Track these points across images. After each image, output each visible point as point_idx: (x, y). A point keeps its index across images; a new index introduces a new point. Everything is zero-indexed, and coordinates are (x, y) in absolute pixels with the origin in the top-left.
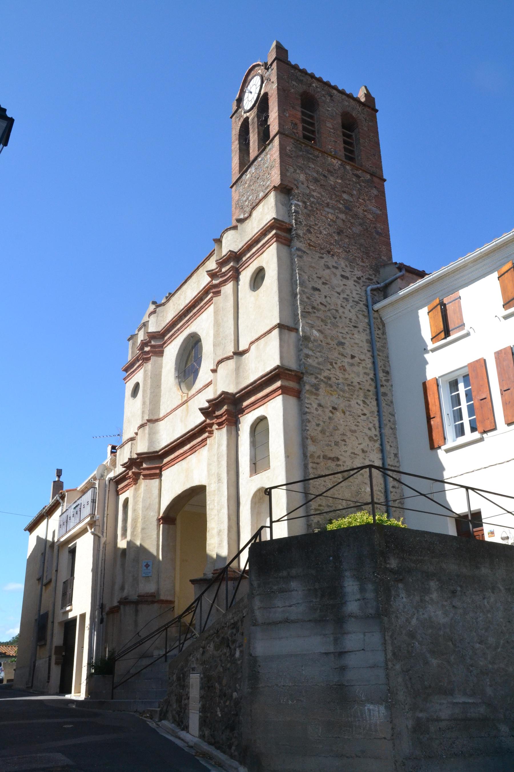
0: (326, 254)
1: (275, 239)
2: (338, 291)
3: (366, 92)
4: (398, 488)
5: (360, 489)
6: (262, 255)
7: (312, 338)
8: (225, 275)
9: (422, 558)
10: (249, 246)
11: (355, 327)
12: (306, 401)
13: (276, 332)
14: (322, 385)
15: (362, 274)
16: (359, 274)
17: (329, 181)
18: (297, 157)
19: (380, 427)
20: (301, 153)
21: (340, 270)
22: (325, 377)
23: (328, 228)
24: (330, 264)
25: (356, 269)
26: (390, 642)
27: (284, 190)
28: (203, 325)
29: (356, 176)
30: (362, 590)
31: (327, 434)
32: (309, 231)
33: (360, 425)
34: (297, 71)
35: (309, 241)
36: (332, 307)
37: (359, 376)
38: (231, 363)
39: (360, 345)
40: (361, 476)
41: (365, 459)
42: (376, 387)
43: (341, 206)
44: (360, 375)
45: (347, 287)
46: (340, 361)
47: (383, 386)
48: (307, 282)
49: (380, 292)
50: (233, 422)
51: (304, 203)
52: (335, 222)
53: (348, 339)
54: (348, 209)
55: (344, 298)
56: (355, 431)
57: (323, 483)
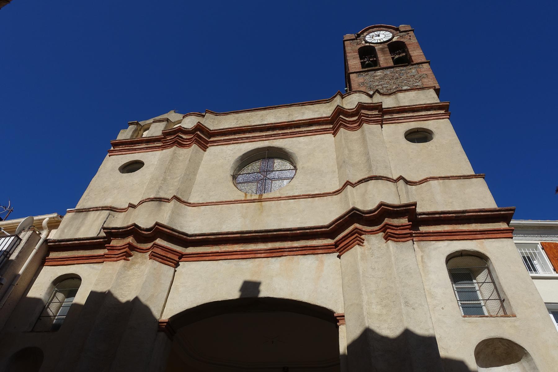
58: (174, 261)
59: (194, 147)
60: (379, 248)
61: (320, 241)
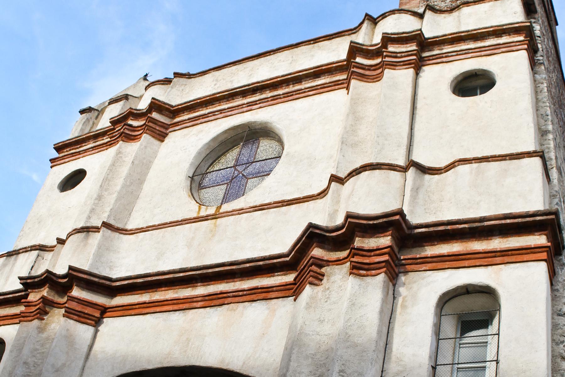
8: (396, 57)
58: (95, 317)
59: (146, 138)
60: (340, 287)
61: (280, 278)
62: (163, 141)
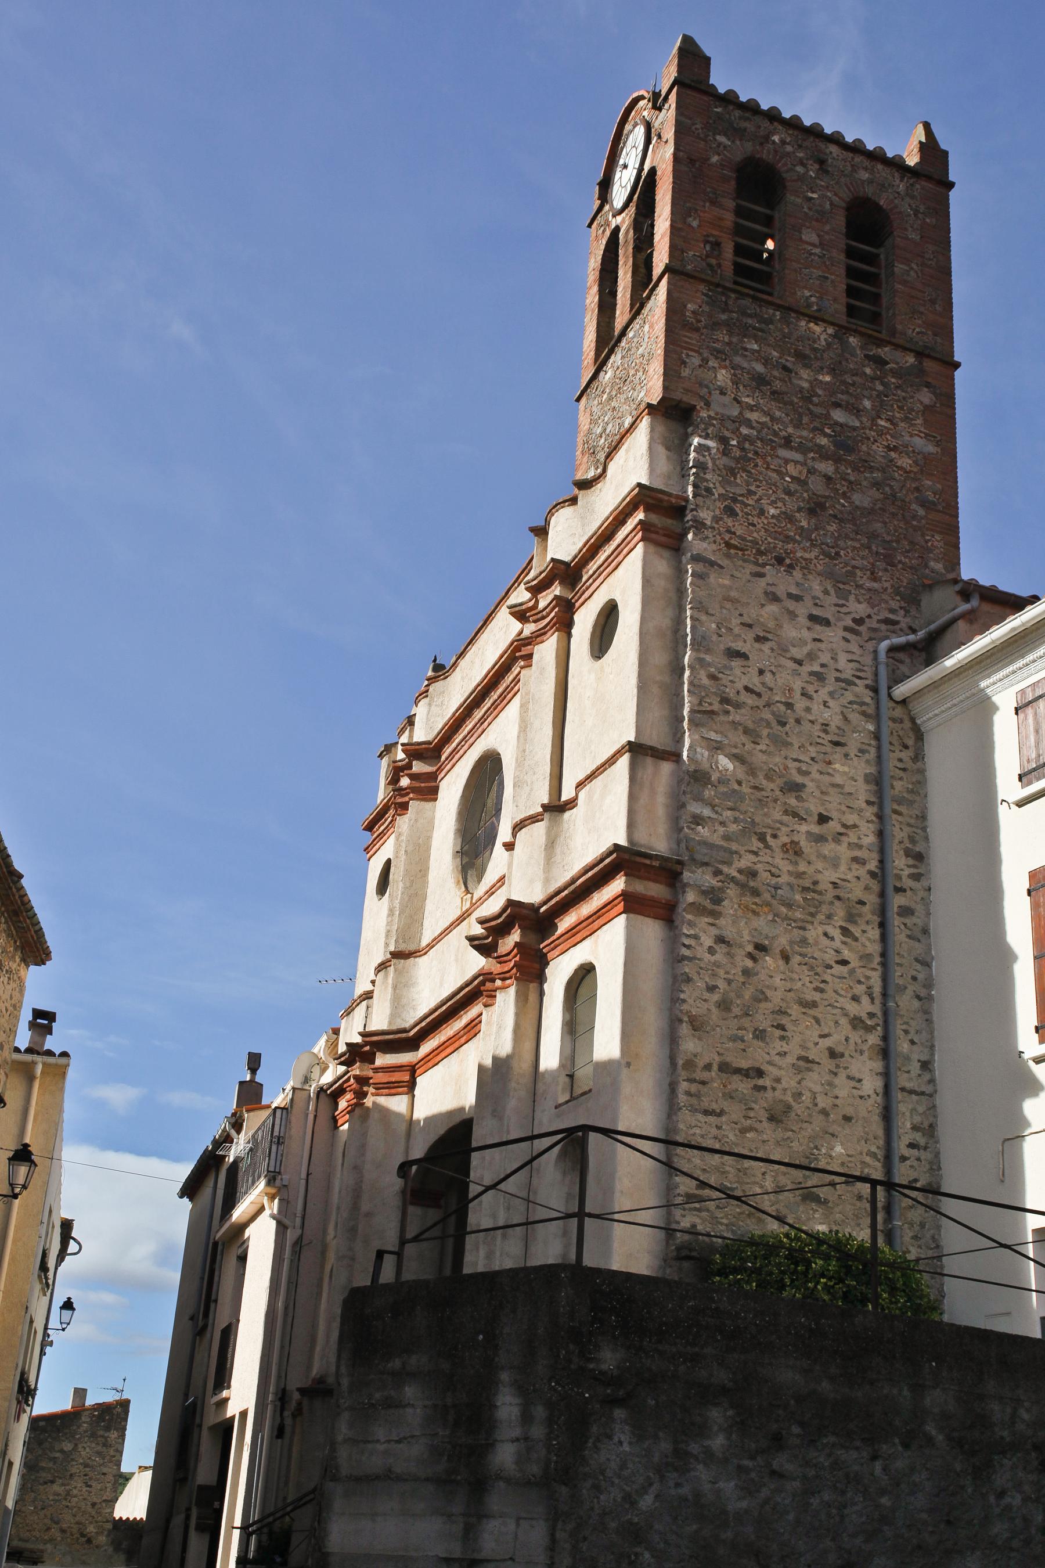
0: (773, 565)
1: (640, 534)
2: (799, 657)
3: (923, 140)
4: (925, 1148)
5: (816, 1147)
6: (616, 572)
7: (714, 777)
8: (544, 618)
9: (697, 1349)
10: (592, 549)
11: (837, 744)
12: (685, 931)
13: (624, 761)
14: (732, 891)
15: (869, 611)
16: (860, 609)
17: (795, 381)
18: (715, 325)
19: (885, 995)
20: (724, 317)
21: (808, 602)
22: (740, 871)
23: (783, 501)
24: (781, 591)
25: (852, 598)
26: (567, 1546)
27: (674, 414)
28: (502, 734)
29: (875, 362)
30: (526, 1418)
31: (736, 1011)
32: (730, 512)
33: (828, 988)
34: (731, 107)
35: (727, 537)
36: (777, 698)
37: (836, 866)
38: (539, 830)
39: (847, 789)
40: (821, 1117)
41: (836, 1074)
42: (882, 894)
43: (824, 441)
44: (841, 866)
45: (822, 646)
46: (788, 829)
47: (905, 891)
48: (715, 638)
49: (916, 653)
50: (531, 969)
51: (723, 441)
52: (803, 483)
53: (815, 775)
54: (845, 446)
55: (812, 674)
56: (814, 1004)
57: (714, 1131)
62: (436, 800)
